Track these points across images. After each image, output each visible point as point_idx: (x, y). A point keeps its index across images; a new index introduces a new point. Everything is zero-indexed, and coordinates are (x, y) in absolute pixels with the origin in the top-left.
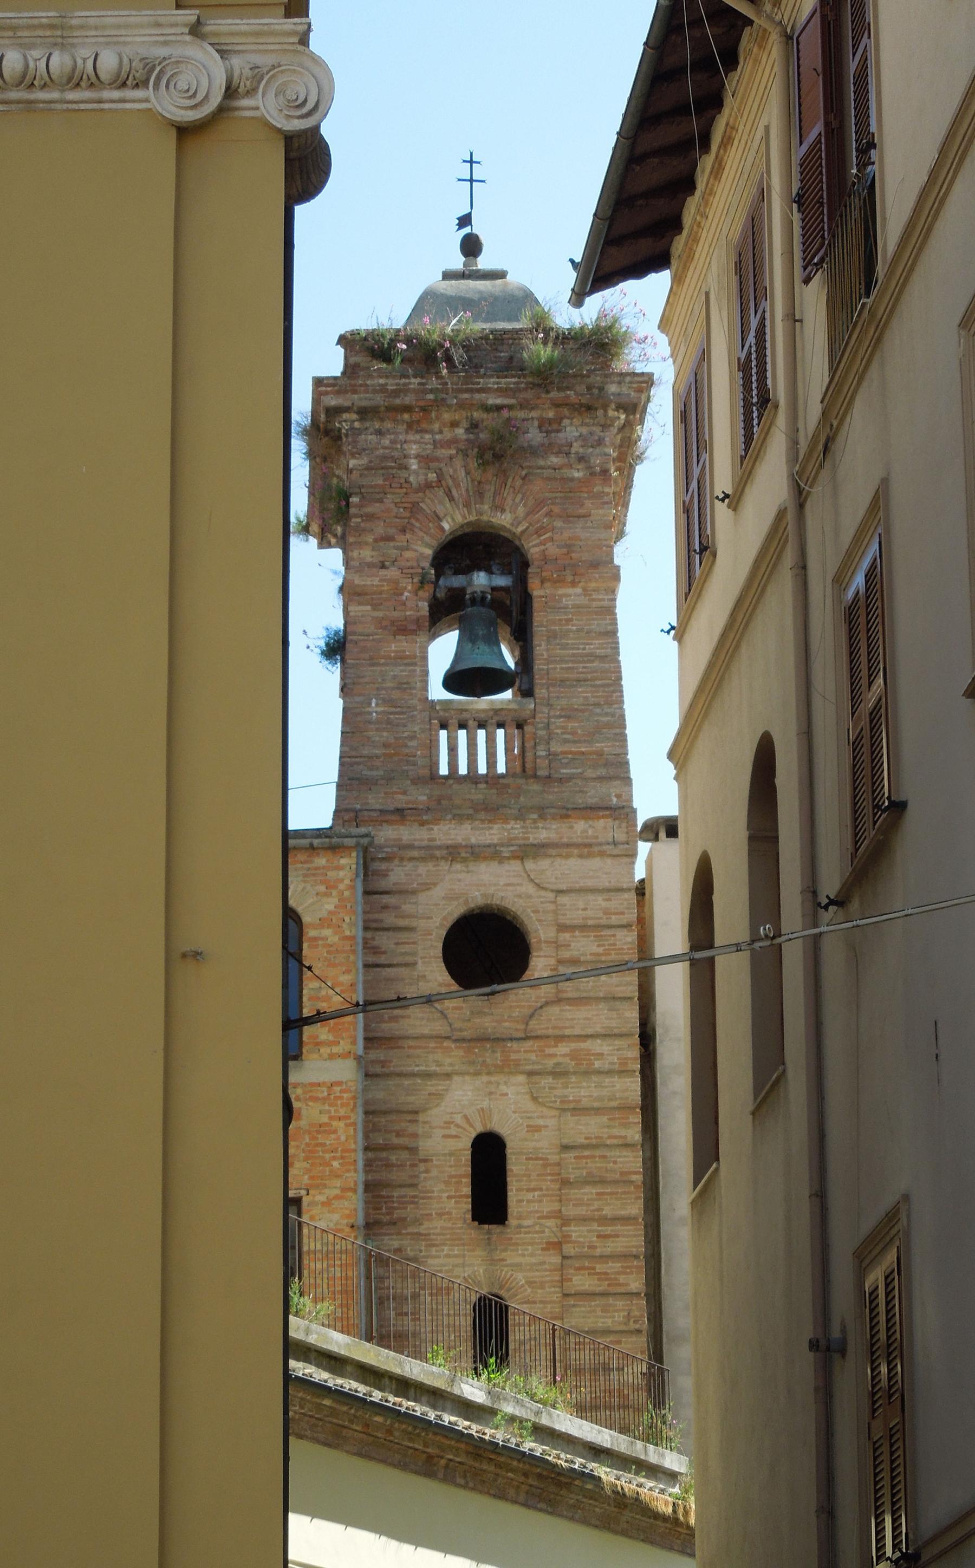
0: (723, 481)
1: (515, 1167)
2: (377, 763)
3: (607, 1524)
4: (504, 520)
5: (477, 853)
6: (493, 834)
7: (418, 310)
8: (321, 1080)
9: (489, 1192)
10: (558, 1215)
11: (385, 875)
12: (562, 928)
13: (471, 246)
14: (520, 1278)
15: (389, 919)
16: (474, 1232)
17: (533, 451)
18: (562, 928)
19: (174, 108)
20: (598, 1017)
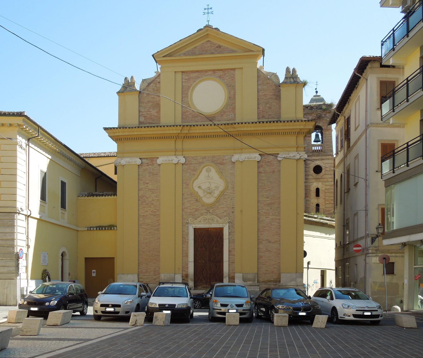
0: (339, 150)
1: (320, 191)
3: (329, 227)
4: (320, 125)
5: (317, 160)
6: (318, 158)
7: (310, 102)
8: (304, 187)
9: (318, 194)
13: (317, 92)
15: (307, 167)
16: (316, 198)
17: (323, 117)
20: (330, 176)
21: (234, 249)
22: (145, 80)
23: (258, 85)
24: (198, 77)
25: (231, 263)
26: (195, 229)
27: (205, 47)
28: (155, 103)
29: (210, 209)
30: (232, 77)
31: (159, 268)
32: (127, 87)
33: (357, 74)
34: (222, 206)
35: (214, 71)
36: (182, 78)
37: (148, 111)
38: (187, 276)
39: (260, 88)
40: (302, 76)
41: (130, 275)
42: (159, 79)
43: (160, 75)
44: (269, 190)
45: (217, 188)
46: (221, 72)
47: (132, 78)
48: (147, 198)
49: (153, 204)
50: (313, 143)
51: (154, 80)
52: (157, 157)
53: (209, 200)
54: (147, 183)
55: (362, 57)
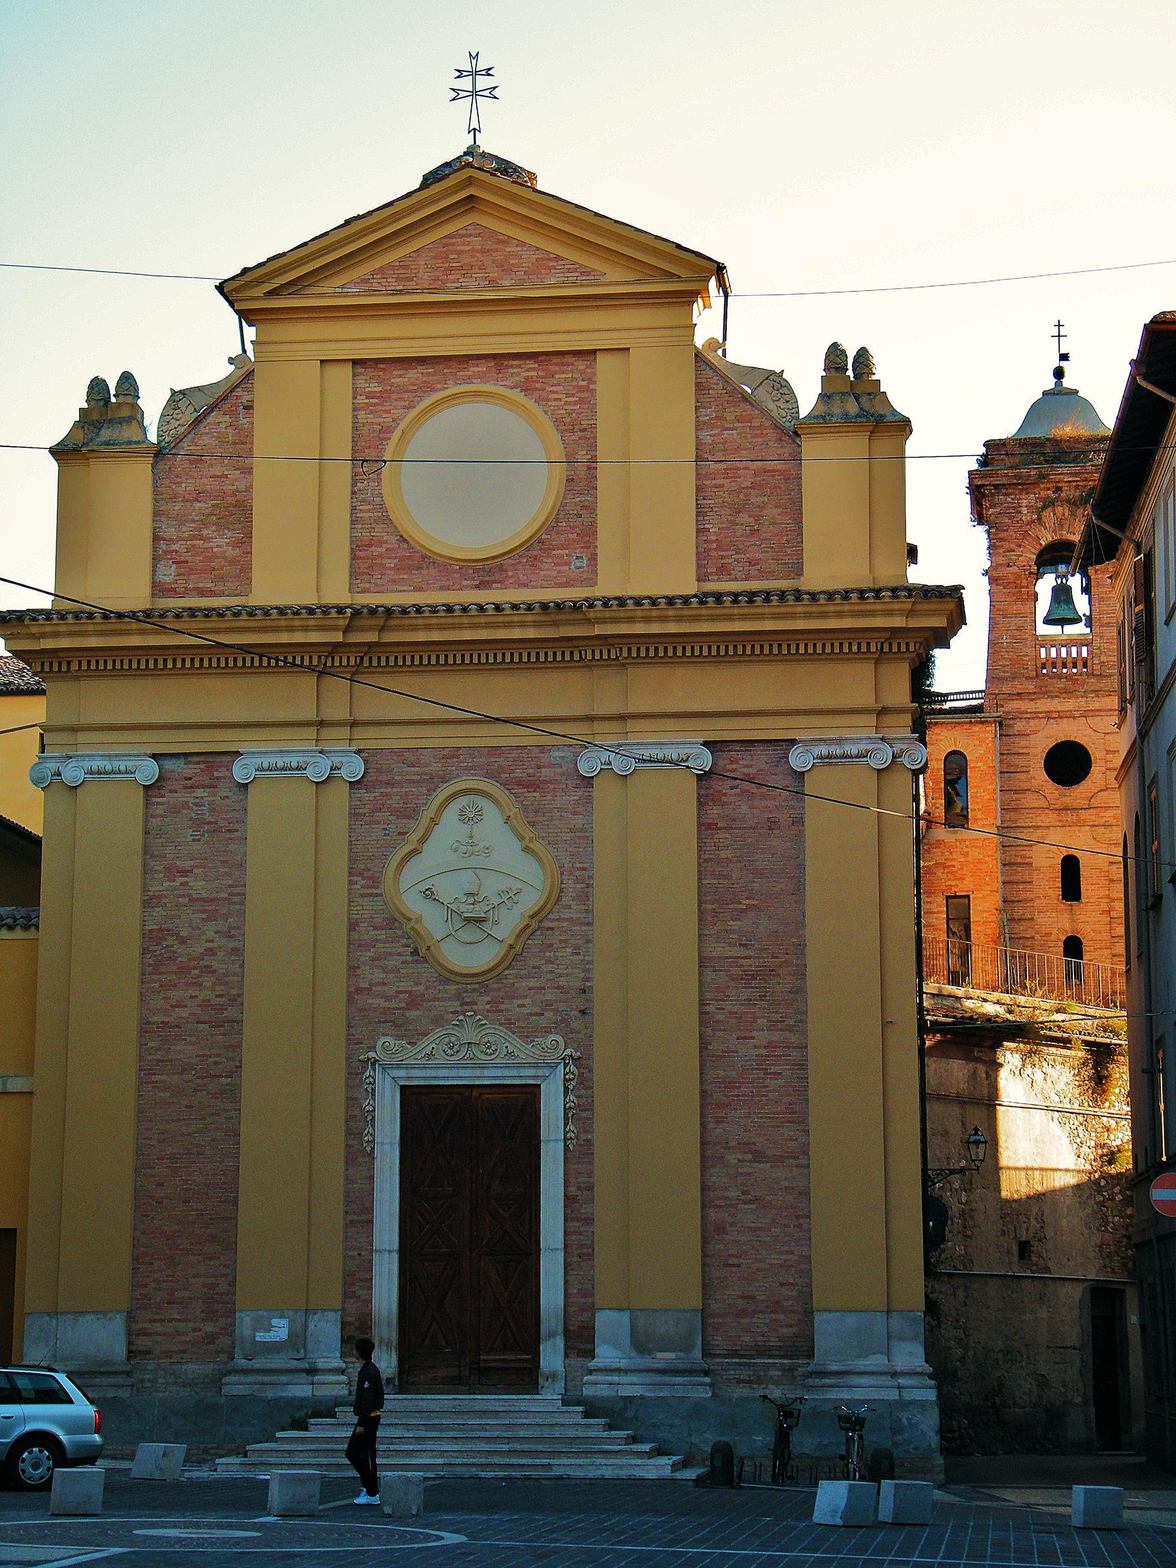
1: (1084, 872)
2: (1007, 669)
6: (1070, 704)
9: (1071, 887)
10: (1108, 897)
11: (1012, 726)
12: (1108, 752)
13: (1059, 373)
14: (1088, 928)
16: (1064, 905)
18: (1108, 752)
19: (875, 764)
21: (590, 1188)
22: (182, 392)
23: (699, 426)
24: (427, 388)
25: (578, 1255)
26: (409, 1094)
27: (460, 253)
28: (230, 500)
29: (482, 990)
30: (581, 389)
31: (233, 1284)
32: (108, 410)
33: (1144, 384)
34: (532, 983)
35: (499, 359)
36: (355, 390)
37: (194, 538)
38: (365, 1322)
39: (709, 440)
40: (899, 388)
41: (89, 1318)
42: (250, 391)
43: (250, 374)
44: (750, 907)
45: (510, 897)
46: (530, 364)
47: (127, 380)
48: (183, 941)
49: (208, 969)
50: (1043, 629)
51: (224, 398)
52: (232, 748)
53: (471, 956)
54: (184, 873)
55: (1155, 321)
